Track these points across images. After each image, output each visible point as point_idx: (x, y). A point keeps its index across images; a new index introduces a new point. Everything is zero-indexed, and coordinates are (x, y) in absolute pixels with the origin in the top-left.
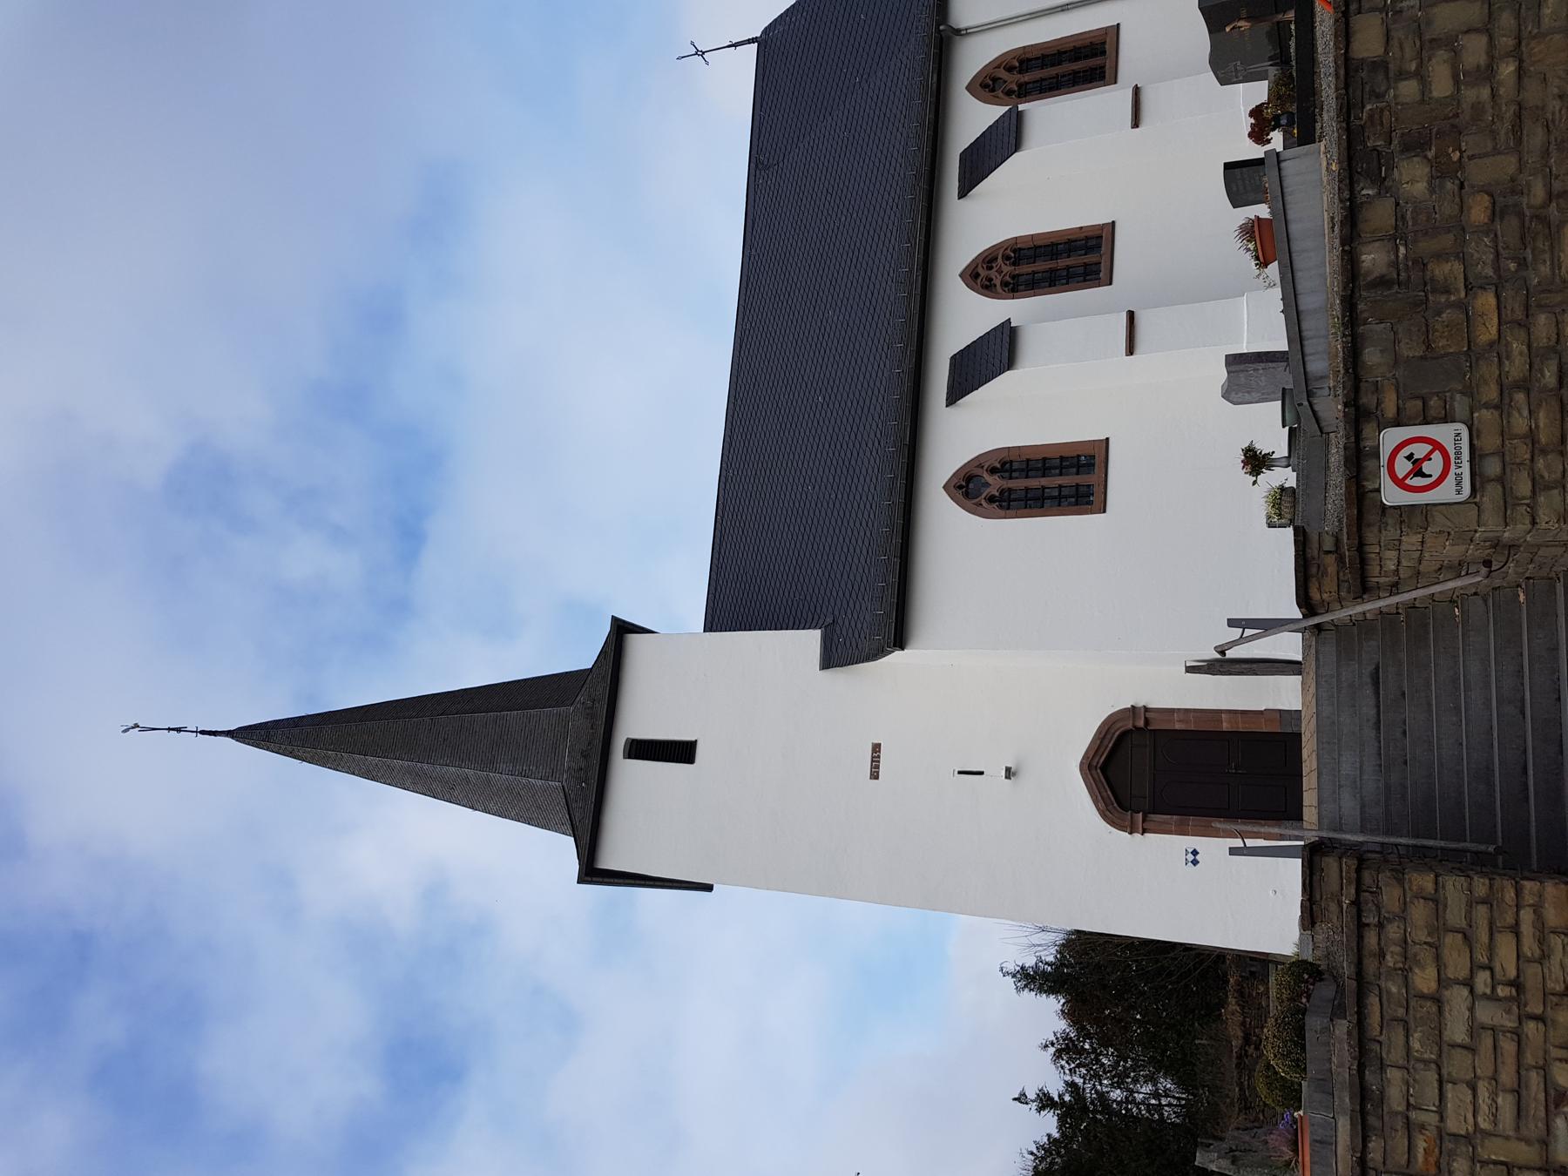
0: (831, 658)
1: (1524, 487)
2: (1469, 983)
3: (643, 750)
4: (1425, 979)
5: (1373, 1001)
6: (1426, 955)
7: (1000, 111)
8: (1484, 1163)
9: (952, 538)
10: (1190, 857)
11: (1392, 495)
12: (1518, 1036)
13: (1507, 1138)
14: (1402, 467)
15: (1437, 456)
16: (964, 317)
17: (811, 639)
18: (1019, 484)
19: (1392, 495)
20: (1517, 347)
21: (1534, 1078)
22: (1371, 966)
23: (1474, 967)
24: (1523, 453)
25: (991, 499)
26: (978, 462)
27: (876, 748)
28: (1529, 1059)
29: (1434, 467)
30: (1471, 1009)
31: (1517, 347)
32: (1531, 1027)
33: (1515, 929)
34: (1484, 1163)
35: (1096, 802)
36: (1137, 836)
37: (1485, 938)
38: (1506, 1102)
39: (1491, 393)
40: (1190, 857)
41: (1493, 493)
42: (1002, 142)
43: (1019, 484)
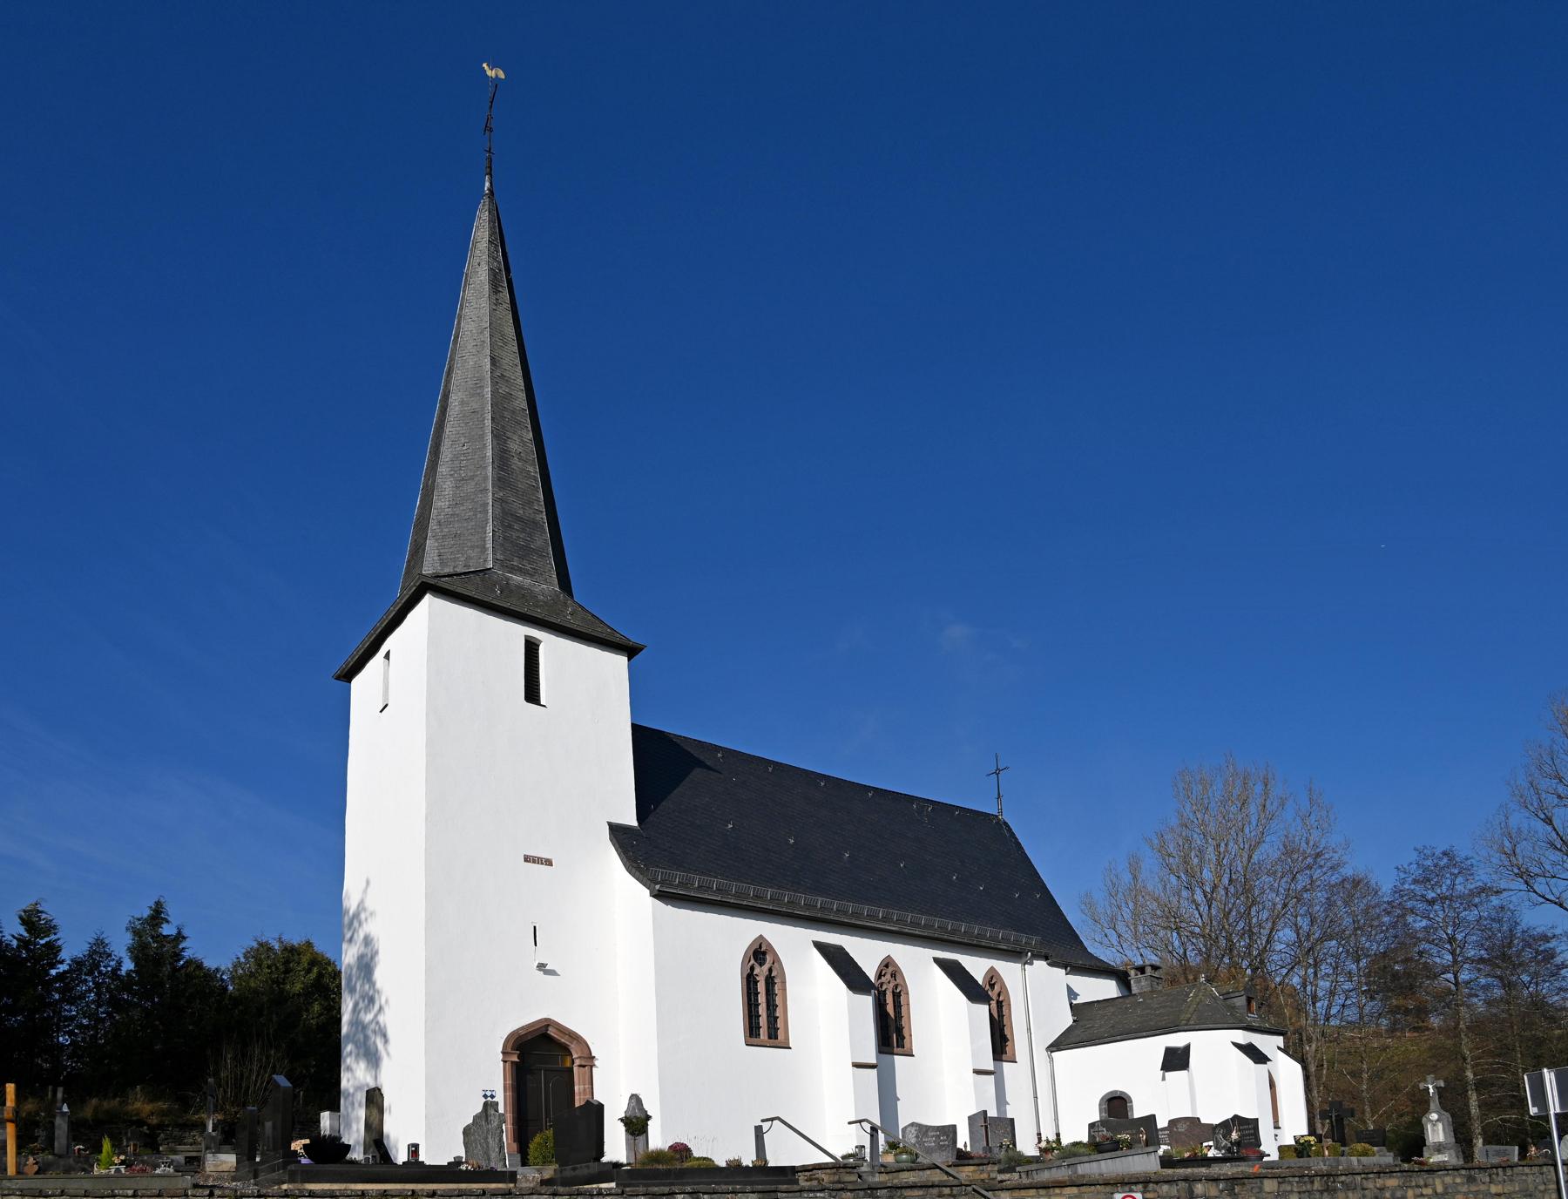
3: (531, 648)
7: (872, 975)
9: (730, 935)
18: (761, 987)
25: (752, 968)
27: (549, 863)
36: (501, 1056)
42: (972, 990)
43: (761, 987)
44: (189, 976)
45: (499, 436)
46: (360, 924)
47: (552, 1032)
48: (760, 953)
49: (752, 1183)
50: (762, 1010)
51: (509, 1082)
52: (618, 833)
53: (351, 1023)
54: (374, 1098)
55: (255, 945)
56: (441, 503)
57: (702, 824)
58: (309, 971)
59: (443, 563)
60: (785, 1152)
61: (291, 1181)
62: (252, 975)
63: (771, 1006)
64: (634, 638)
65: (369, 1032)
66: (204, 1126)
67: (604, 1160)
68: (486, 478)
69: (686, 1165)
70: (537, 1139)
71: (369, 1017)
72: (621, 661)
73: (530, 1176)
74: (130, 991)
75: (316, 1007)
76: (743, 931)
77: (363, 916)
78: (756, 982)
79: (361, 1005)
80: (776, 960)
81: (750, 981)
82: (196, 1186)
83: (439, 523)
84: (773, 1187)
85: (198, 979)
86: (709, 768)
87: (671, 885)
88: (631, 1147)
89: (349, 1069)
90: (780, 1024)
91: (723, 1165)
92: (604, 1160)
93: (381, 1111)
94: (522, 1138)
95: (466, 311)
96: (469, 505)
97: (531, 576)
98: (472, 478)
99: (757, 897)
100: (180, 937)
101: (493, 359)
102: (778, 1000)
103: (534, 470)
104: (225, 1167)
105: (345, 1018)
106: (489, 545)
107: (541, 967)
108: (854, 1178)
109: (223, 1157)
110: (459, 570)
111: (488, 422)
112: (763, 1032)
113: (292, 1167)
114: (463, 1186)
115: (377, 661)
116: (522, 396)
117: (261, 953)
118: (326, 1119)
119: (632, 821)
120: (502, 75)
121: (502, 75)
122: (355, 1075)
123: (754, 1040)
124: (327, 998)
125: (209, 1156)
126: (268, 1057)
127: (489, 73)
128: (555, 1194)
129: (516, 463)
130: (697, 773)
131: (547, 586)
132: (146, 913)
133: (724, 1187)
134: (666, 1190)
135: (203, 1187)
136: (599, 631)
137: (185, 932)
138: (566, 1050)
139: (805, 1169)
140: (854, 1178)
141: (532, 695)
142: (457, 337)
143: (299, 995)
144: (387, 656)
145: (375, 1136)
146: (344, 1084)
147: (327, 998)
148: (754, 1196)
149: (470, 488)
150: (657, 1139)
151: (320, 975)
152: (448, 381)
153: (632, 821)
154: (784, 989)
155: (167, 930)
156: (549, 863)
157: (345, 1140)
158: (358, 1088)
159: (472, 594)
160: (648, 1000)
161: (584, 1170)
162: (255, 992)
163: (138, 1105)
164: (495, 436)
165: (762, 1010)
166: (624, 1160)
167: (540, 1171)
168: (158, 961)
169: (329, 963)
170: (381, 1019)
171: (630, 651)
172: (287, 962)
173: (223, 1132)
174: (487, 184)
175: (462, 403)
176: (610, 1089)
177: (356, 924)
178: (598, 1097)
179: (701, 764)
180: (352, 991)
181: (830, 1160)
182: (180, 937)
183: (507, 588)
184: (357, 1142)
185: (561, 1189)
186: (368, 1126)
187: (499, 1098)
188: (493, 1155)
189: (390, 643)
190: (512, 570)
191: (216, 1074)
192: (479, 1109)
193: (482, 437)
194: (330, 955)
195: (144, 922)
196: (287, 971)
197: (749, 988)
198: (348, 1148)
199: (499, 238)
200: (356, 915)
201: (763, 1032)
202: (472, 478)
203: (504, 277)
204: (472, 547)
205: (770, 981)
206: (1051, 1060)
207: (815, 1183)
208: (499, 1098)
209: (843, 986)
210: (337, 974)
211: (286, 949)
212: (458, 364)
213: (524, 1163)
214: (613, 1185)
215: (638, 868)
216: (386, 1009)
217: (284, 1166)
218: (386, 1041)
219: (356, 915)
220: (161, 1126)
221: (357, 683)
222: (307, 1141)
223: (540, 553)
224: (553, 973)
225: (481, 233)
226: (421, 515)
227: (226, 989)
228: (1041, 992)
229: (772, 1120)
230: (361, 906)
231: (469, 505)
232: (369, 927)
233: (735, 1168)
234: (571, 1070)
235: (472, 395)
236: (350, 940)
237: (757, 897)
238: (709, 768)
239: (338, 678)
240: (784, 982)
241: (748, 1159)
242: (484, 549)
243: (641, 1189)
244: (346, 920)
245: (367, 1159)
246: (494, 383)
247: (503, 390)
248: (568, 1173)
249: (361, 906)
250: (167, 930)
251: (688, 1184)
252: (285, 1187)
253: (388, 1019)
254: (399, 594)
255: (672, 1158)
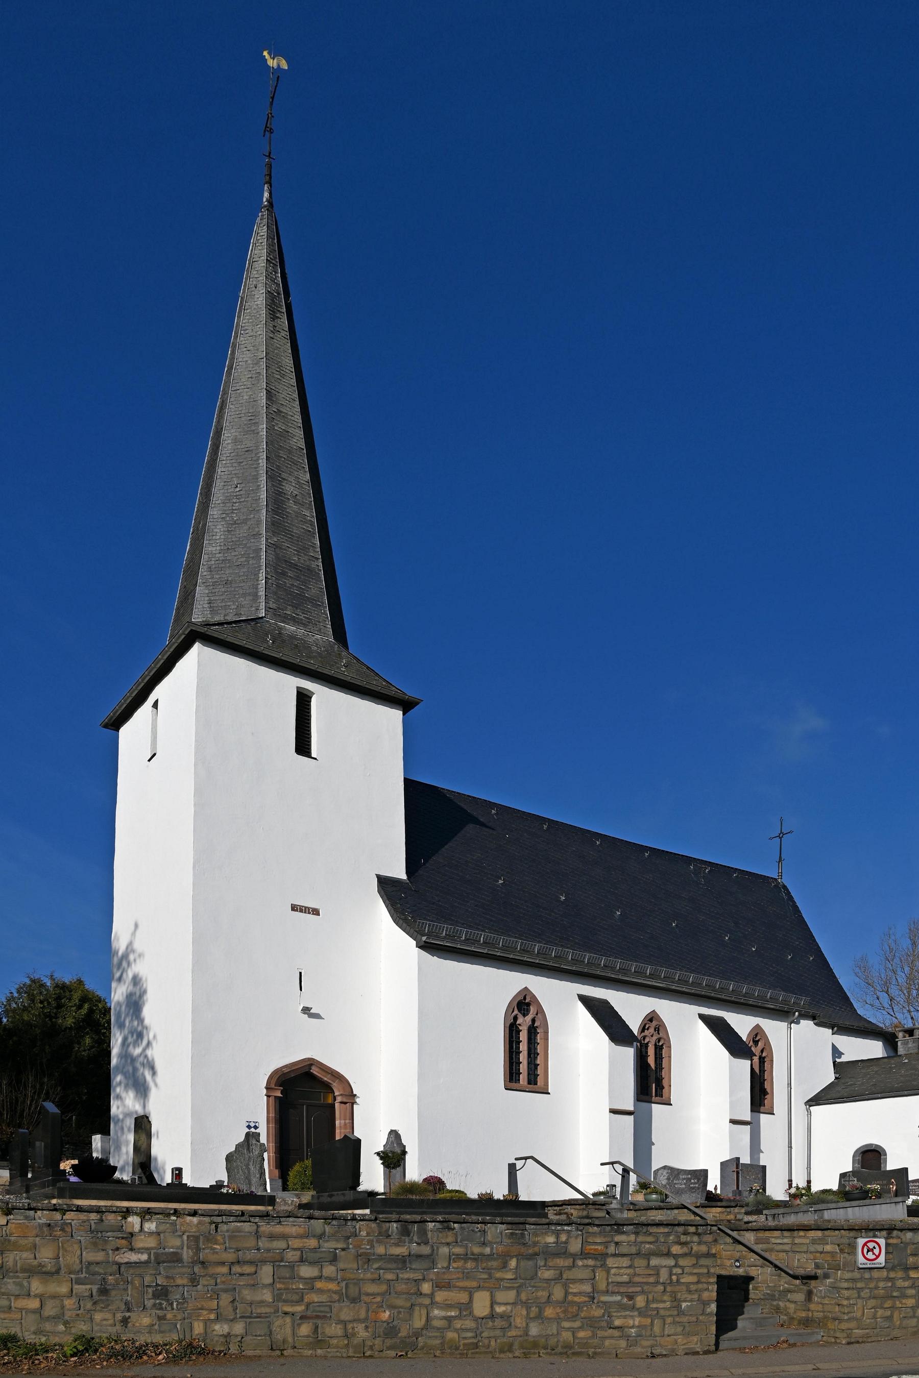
0: (387, 887)
1: (859, 1285)
2: (676, 1266)
3: (303, 700)
4: (676, 1249)
5: (666, 1230)
6: (685, 1250)
7: (636, 1032)
8: (593, 1271)
9: (491, 989)
10: (252, 1125)
11: (861, 1241)
12: (657, 1283)
13: (607, 1279)
14: (871, 1245)
15: (874, 1257)
16: (632, 1008)
17: (400, 873)
18: (524, 1036)
19: (861, 1241)
20: (906, 1284)
21: (639, 1289)
22: (680, 1229)
23: (682, 1268)
24: (872, 1285)
25: (515, 1018)
26: (540, 1011)
27: (316, 912)
28: (646, 1288)
29: (870, 1256)
30: (665, 1266)
31: (906, 1284)
32: (661, 1288)
33: (698, 1282)
34: (593, 1271)
35: (286, 1066)
37: (695, 1271)
38: (625, 1278)
39: (892, 1275)
40: (252, 1125)
41: (856, 1275)
43: (524, 1036)
201: (523, 1078)
206: (809, 1113)
228: (804, 1050)
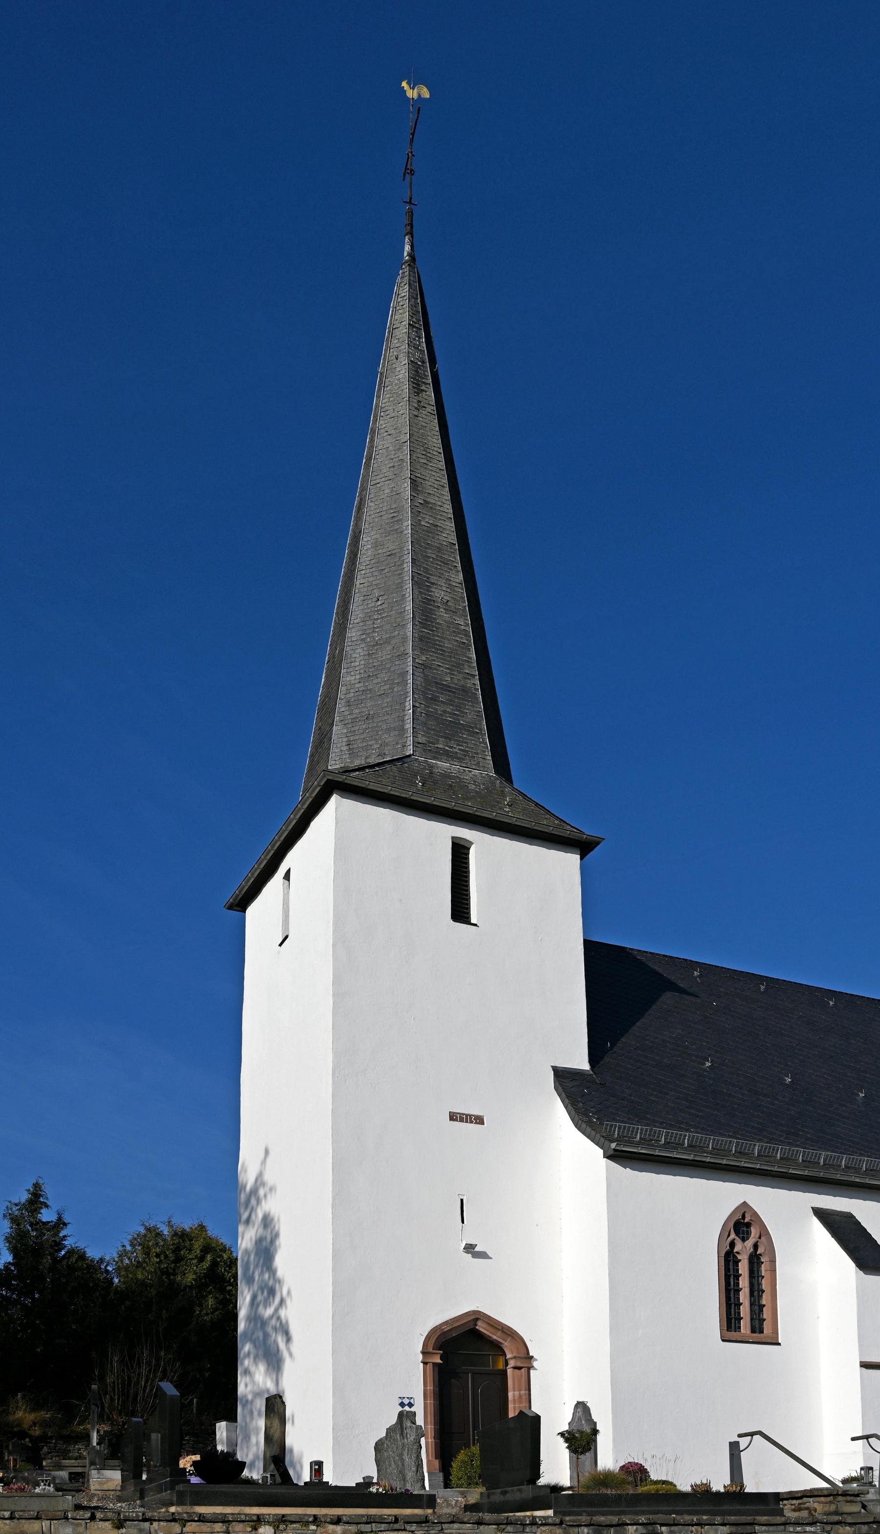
3: (460, 853)
18: (743, 1268)
25: (732, 1244)
27: (479, 1120)
36: (421, 1357)
43: (743, 1268)
44: (71, 1268)
45: (421, 583)
46: (258, 1201)
47: (481, 1327)
48: (742, 1224)
49: (723, 1514)
50: (744, 1297)
51: (430, 1388)
52: (564, 1078)
53: (249, 1319)
54: (275, 1406)
55: (142, 1230)
56: (349, 678)
57: (667, 1064)
58: (201, 1259)
59: (353, 753)
60: (765, 1475)
61: (180, 1503)
62: (139, 1265)
63: (756, 1291)
64: (589, 831)
65: (269, 1330)
66: (87, 1438)
67: (542, 1481)
68: (404, 639)
69: (641, 1489)
70: (462, 1456)
71: (269, 1311)
72: (573, 860)
73: (451, 1500)
74: (9, 1287)
75: (211, 1301)
76: (724, 1196)
77: (261, 1192)
78: (737, 1262)
79: (259, 1298)
80: (764, 1232)
81: (729, 1260)
82: (78, 1507)
83: (348, 704)
84: (749, 1519)
85: (81, 1271)
86: (682, 991)
87: (630, 1143)
88: (575, 1466)
89: (247, 1372)
90: (766, 1313)
91: (689, 1489)
92: (542, 1481)
93: (283, 1421)
94: (445, 1454)
95: (382, 423)
96: (384, 676)
97: (460, 760)
98: (387, 641)
99: (740, 1153)
100: (60, 1223)
101: (413, 482)
102: (765, 1284)
103: (465, 622)
104: (111, 1486)
105: (243, 1313)
106: (409, 726)
107: (469, 1248)
108: (856, 1508)
109: (108, 1473)
110: (373, 760)
111: (408, 567)
112: (745, 1325)
113: (180, 1487)
114: (373, 1511)
115: (276, 881)
116: (450, 526)
117: (149, 1239)
118: (222, 1429)
119: (582, 1063)
120: (426, 94)
121: (426, 94)
122: (253, 1380)
123: (733, 1335)
124: (222, 1290)
125: (94, 1473)
126: (158, 1360)
127: (412, 94)
128: (479, 1523)
129: (442, 616)
130: (668, 998)
131: (484, 770)
132: (24, 1197)
133: (687, 1518)
134: (615, 1519)
135: (85, 1508)
136: (546, 825)
137: (66, 1218)
138: (498, 1349)
139: (792, 1496)
140: (856, 1508)
141: (460, 911)
142: (369, 459)
143: (191, 1287)
144: (287, 876)
145: (275, 1451)
146: (241, 1389)
147: (222, 1290)
148: (726, 1529)
149: (384, 654)
150: (608, 1458)
151: (214, 1264)
152: (358, 519)
153: (582, 1063)
154: (773, 1270)
155: (47, 1216)
156: (479, 1120)
157: (240, 1457)
158: (257, 1394)
159: (387, 790)
160: (585, 1268)
161: (515, 1494)
162: (143, 1284)
163: (20, 1414)
164: (417, 583)
165: (744, 1297)
166: (566, 1481)
167: (463, 1494)
168: (37, 1251)
169: (224, 1249)
170: (282, 1313)
171: (583, 846)
172: (177, 1249)
173: (111, 1445)
174: (407, 248)
175: (376, 545)
176: (551, 1399)
177: (253, 1201)
178: (536, 1408)
179: (671, 986)
180: (250, 1281)
181: (825, 1485)
182: (60, 1223)
183: (431, 779)
184: (257, 1457)
185: (487, 1517)
186: (268, 1438)
187: (419, 1409)
188: (410, 1475)
189: (290, 860)
190: (438, 754)
191: (102, 1379)
192: (393, 1420)
193: (400, 586)
194: (225, 1240)
195: (23, 1207)
196: (178, 1260)
197: (727, 1269)
198: (242, 1465)
199: (422, 319)
200: (254, 1191)
201: (745, 1325)
202: (387, 641)
203: (429, 371)
204: (389, 730)
205: (755, 1260)
207: (804, 1514)
208: (419, 1409)
209: (850, 1264)
210: (233, 1262)
211: (175, 1234)
212: (371, 490)
213: (447, 1485)
214: (550, 1513)
215: (589, 1123)
216: (288, 1302)
217: (172, 1486)
218: (288, 1339)
219: (254, 1191)
220: (44, 1438)
221: (253, 912)
222: (197, 1458)
223: (471, 730)
224: (483, 1255)
225: (400, 315)
226: (326, 695)
227: (111, 1282)
229: (752, 1434)
230: (260, 1181)
231: (384, 676)
232: (270, 1205)
233: (702, 1498)
234: (504, 1373)
235: (389, 534)
236: (248, 1221)
237: (740, 1153)
238: (682, 991)
239: (231, 907)
240: (773, 1261)
241: (720, 1482)
242: (402, 730)
243: (584, 1519)
244: (243, 1197)
245: (264, 1478)
246: (415, 513)
247: (427, 520)
248: (497, 1497)
249: (260, 1181)
250: (47, 1216)
251: (643, 1513)
252: (173, 1509)
253: (291, 1314)
254: (301, 798)
255: (623, 1482)
